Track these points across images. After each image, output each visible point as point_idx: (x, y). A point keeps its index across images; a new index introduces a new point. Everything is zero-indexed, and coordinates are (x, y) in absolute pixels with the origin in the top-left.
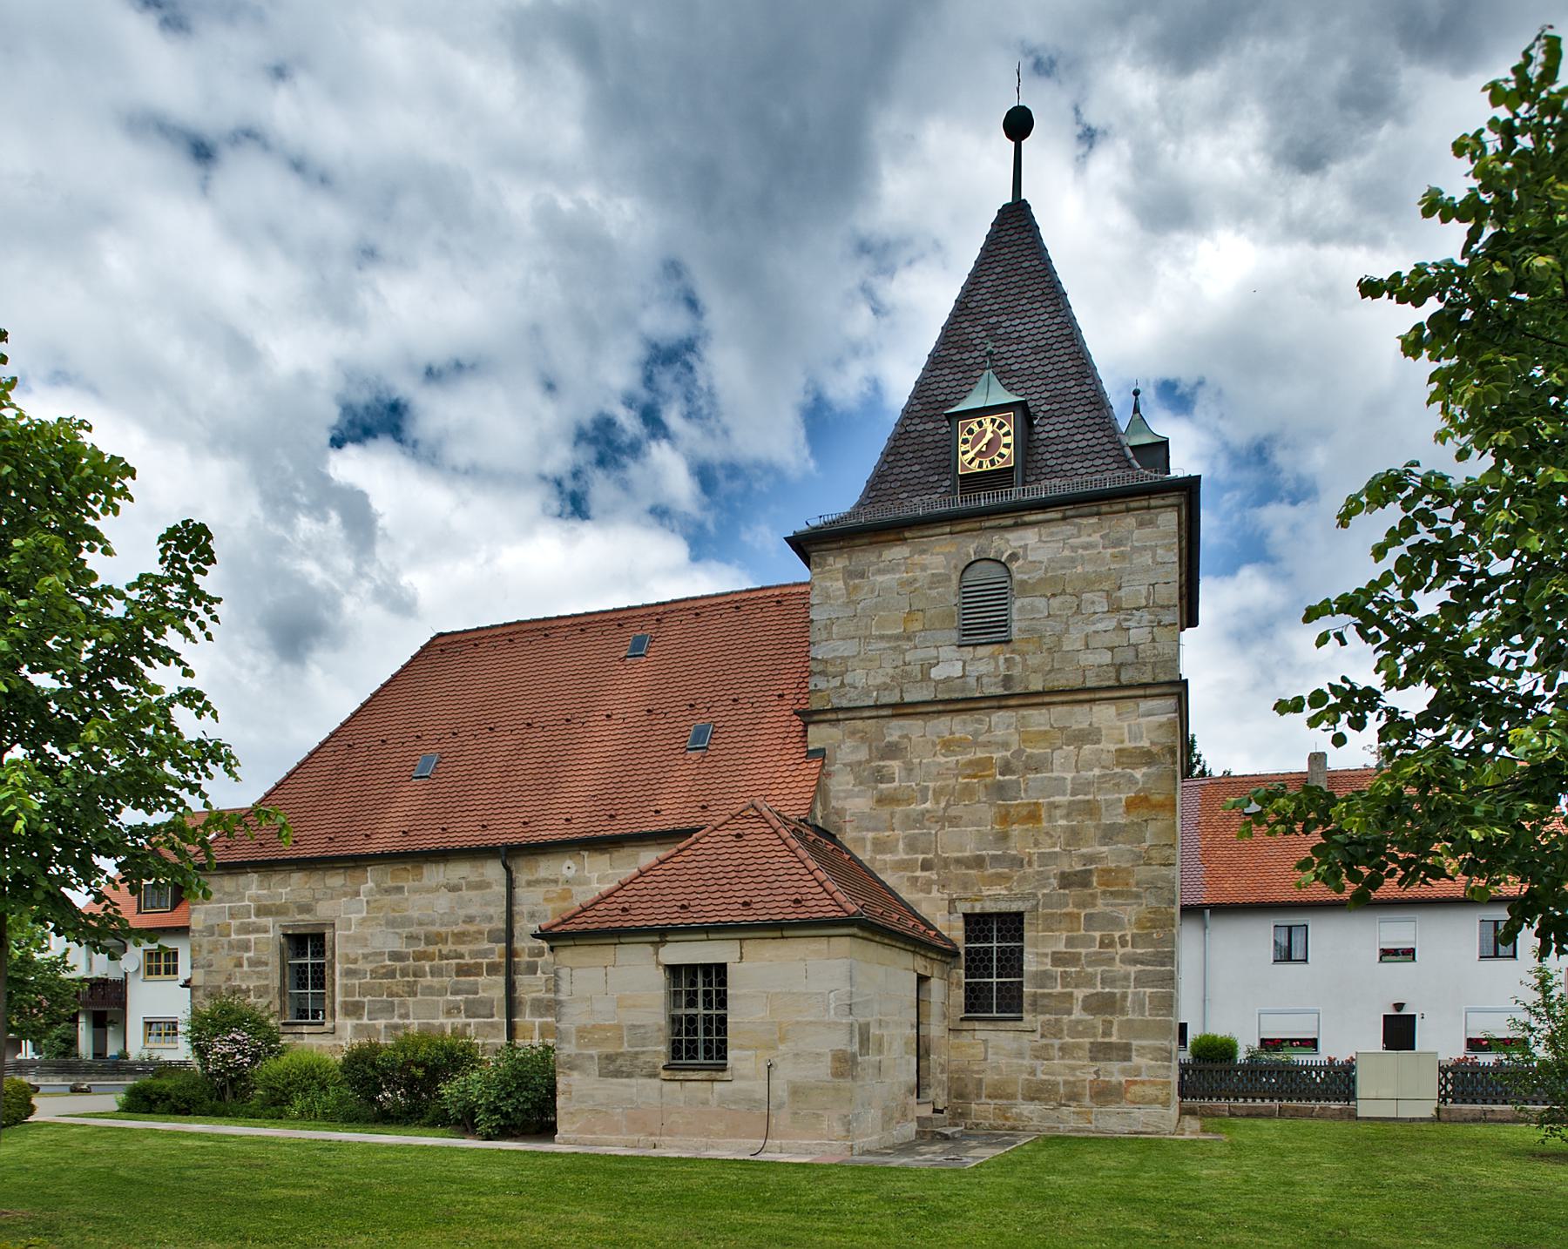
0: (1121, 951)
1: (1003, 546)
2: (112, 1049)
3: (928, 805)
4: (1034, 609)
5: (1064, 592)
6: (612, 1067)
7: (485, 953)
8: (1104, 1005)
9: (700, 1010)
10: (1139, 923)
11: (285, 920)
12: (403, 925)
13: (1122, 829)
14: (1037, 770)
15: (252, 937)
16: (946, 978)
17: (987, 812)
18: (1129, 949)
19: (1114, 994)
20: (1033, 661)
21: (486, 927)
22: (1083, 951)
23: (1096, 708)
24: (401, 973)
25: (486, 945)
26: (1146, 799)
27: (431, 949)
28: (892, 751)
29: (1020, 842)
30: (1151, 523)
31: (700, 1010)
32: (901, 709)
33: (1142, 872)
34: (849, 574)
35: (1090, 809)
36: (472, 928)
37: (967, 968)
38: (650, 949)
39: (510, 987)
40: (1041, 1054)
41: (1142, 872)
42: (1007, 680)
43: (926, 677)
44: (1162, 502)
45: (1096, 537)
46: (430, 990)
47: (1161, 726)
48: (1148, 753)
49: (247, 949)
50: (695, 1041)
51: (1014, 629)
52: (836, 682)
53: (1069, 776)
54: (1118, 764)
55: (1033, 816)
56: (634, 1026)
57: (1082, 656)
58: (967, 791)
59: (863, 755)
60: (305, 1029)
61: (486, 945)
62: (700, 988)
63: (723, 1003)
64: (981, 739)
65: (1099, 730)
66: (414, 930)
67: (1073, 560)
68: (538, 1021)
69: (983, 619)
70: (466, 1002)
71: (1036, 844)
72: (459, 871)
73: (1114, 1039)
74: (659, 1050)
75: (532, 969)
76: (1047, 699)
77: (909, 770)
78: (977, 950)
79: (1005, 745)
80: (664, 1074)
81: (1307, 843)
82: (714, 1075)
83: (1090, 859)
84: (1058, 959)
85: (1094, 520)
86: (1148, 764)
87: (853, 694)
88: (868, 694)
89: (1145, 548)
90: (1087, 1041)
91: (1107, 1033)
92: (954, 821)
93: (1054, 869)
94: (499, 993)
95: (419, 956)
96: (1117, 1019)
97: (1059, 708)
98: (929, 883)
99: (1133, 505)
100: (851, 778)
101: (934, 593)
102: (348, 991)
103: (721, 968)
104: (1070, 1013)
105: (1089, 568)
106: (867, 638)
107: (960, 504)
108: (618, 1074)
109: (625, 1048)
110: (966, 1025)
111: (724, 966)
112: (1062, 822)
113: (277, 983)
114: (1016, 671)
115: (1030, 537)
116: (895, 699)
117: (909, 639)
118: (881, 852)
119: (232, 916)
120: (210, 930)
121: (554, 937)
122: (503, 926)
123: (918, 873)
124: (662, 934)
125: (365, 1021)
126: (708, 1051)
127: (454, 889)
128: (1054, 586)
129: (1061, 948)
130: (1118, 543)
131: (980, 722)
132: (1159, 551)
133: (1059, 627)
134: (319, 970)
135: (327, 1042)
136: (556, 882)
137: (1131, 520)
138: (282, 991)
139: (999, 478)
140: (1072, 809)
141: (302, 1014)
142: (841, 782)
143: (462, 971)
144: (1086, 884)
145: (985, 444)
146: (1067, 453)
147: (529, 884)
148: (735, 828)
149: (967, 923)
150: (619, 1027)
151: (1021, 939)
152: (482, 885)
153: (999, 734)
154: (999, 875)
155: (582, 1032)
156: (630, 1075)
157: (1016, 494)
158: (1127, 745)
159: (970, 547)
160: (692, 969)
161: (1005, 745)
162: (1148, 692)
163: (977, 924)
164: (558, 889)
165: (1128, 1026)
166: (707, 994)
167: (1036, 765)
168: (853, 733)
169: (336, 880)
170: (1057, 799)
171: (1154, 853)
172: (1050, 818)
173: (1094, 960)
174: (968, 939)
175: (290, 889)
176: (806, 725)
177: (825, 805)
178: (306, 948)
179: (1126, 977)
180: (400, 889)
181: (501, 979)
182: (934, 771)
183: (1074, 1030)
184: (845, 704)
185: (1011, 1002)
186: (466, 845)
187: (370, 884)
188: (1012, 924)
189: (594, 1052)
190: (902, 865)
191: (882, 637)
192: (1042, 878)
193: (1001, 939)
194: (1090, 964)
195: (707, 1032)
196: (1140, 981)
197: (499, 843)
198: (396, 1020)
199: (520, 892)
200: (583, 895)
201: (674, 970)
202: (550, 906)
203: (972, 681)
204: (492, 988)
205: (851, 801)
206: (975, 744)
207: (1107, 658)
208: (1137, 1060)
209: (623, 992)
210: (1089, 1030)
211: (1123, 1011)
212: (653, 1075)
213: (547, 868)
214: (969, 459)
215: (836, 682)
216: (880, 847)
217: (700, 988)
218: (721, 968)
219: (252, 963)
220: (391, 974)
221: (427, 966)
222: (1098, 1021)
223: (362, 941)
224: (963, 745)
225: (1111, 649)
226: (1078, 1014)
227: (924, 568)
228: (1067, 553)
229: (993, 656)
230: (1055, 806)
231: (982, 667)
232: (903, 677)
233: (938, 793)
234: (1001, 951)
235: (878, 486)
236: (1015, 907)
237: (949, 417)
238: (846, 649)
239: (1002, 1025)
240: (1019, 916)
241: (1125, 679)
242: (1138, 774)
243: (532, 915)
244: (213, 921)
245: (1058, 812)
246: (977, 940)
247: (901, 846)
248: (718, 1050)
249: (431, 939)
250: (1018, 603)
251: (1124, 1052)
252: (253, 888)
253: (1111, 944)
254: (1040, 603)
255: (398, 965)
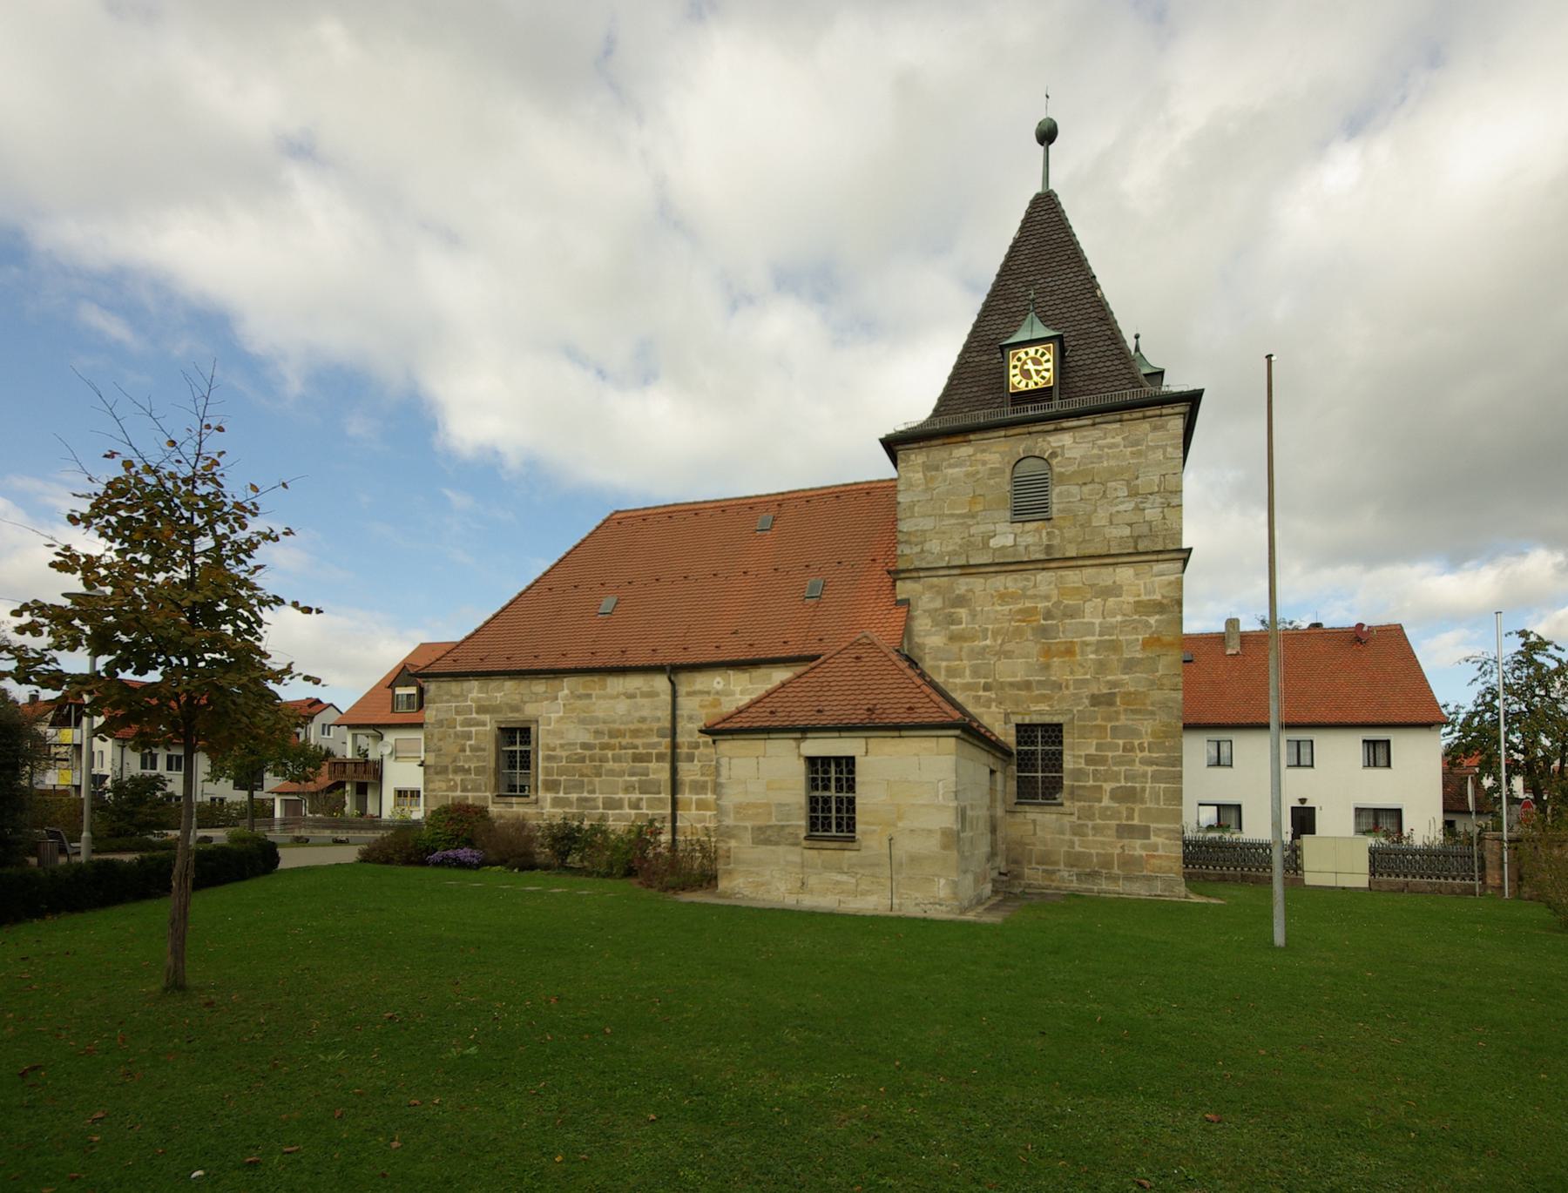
0: (1140, 755)
1: (1045, 445)
2: (372, 809)
3: (988, 642)
4: (1070, 495)
5: (1093, 481)
6: (764, 836)
7: (654, 745)
8: (1127, 796)
9: (833, 793)
10: (1154, 734)
11: (500, 717)
12: (591, 723)
13: (1139, 661)
14: (1072, 617)
15: (473, 729)
16: (1004, 773)
17: (1033, 647)
18: (1146, 754)
19: (1134, 788)
20: (1069, 533)
21: (655, 726)
22: (1110, 754)
23: (1118, 570)
24: (589, 760)
25: (656, 740)
26: (1159, 639)
27: (613, 741)
28: (961, 601)
29: (1060, 670)
30: (1162, 427)
31: (833, 793)
32: (967, 569)
33: (1157, 695)
34: (926, 468)
35: (1114, 647)
36: (644, 727)
37: (1019, 765)
38: (793, 743)
39: (674, 771)
40: (1078, 831)
41: (1157, 695)
42: (1049, 547)
43: (986, 545)
44: (1170, 411)
45: (1118, 439)
46: (611, 773)
47: (1170, 583)
48: (1160, 604)
49: (470, 738)
50: (829, 818)
51: (1055, 508)
52: (917, 549)
53: (1097, 621)
54: (1136, 612)
55: (1069, 651)
56: (780, 805)
57: (1107, 530)
58: (1018, 632)
59: (938, 604)
60: (514, 800)
61: (656, 740)
62: (833, 775)
63: (851, 788)
64: (1029, 593)
65: (1121, 587)
66: (600, 726)
67: (1100, 457)
68: (694, 797)
69: (1029, 500)
70: (640, 782)
71: (1072, 673)
72: (635, 683)
73: (1136, 822)
74: (801, 822)
75: (691, 758)
76: (1080, 563)
77: (973, 615)
78: (1026, 753)
79: (1047, 598)
80: (805, 843)
81: (1522, 640)
82: (845, 845)
83: (1114, 684)
84: (1090, 760)
85: (1117, 425)
86: (1161, 613)
87: (930, 558)
88: (942, 558)
89: (1158, 447)
90: (1114, 822)
91: (1130, 817)
92: (1008, 655)
93: (1086, 692)
94: (665, 776)
95: (604, 747)
96: (1137, 807)
97: (1090, 570)
98: (990, 700)
99: (1149, 413)
100: (929, 621)
101: (992, 482)
102: (548, 771)
103: (851, 760)
104: (1100, 801)
105: (1113, 463)
106: (942, 516)
107: (1009, 414)
108: (767, 842)
109: (773, 822)
110: (1019, 808)
111: (853, 758)
112: (1092, 656)
113: (493, 764)
114: (1056, 542)
115: (1066, 439)
116: (963, 562)
117: (973, 517)
118: (954, 676)
119: (458, 713)
120: (440, 723)
121: (715, 732)
122: (668, 725)
123: (981, 693)
124: (804, 731)
125: (561, 794)
126: (839, 825)
127: (631, 696)
128: (1085, 477)
129: (1093, 751)
130: (1136, 443)
131: (1028, 580)
132: (1169, 449)
133: (1089, 508)
134: (526, 755)
135: (531, 810)
136: (708, 693)
137: (1146, 426)
138: (497, 770)
139: (1041, 395)
140: (1100, 646)
141: (512, 788)
142: (922, 624)
143: (637, 758)
144: (1111, 703)
145: (1032, 368)
146: (1091, 377)
147: (689, 694)
148: (854, 652)
149: (1018, 731)
150: (768, 805)
151: (1061, 743)
152: (652, 694)
153: (1043, 589)
154: (1044, 696)
155: (739, 808)
156: (777, 844)
157: (1056, 406)
158: (1144, 598)
159: (1021, 446)
160: (826, 760)
161: (1047, 598)
162: (1161, 557)
163: (1025, 732)
164: (710, 698)
165: (1146, 813)
166: (838, 780)
167: (1072, 613)
168: (931, 587)
169: (539, 687)
170: (1088, 639)
171: (1165, 681)
172: (1083, 653)
173: (1119, 762)
174: (1019, 743)
175: (503, 693)
176: (895, 581)
177: (910, 640)
178: (516, 741)
179: (1144, 775)
180: (589, 696)
181: (667, 765)
182: (992, 616)
183: (1104, 813)
184: (924, 565)
185: (1052, 789)
186: (640, 664)
187: (566, 691)
188: (1054, 732)
189: (749, 824)
190: (967, 687)
191: (952, 515)
192: (1077, 699)
193: (1045, 743)
194: (1115, 764)
195: (838, 810)
196: (1156, 778)
197: (665, 663)
198: (585, 795)
199: (680, 700)
200: (729, 706)
201: (812, 761)
202: (704, 711)
203: (1021, 549)
204: (661, 772)
205: (930, 638)
206: (1024, 596)
207: (1127, 531)
208: (1153, 839)
209: (771, 775)
210: (1116, 814)
211: (1142, 801)
212: (796, 844)
213: (702, 681)
214: (1017, 382)
215: (917, 549)
216: (952, 672)
217: (833, 775)
218: (851, 760)
219: (473, 749)
220: (582, 760)
221: (610, 754)
222: (1123, 808)
223: (558, 734)
224: (1014, 597)
225: (1130, 525)
226: (1106, 802)
227: (984, 463)
228: (1095, 451)
229: (1037, 530)
230: (1086, 644)
231: (1030, 538)
232: (968, 544)
233: (995, 634)
234: (1045, 753)
235: (946, 402)
236: (1056, 720)
237: (1002, 348)
238: (928, 524)
239: (1047, 809)
240: (1059, 726)
241: (1141, 548)
242: (1152, 620)
243: (690, 718)
244: (442, 716)
245: (1089, 649)
246: (1026, 743)
247: (968, 672)
248: (848, 824)
249: (613, 734)
250: (1057, 490)
251: (1145, 832)
252: (474, 691)
253: (1132, 749)
254: (1075, 489)
255: (587, 753)
